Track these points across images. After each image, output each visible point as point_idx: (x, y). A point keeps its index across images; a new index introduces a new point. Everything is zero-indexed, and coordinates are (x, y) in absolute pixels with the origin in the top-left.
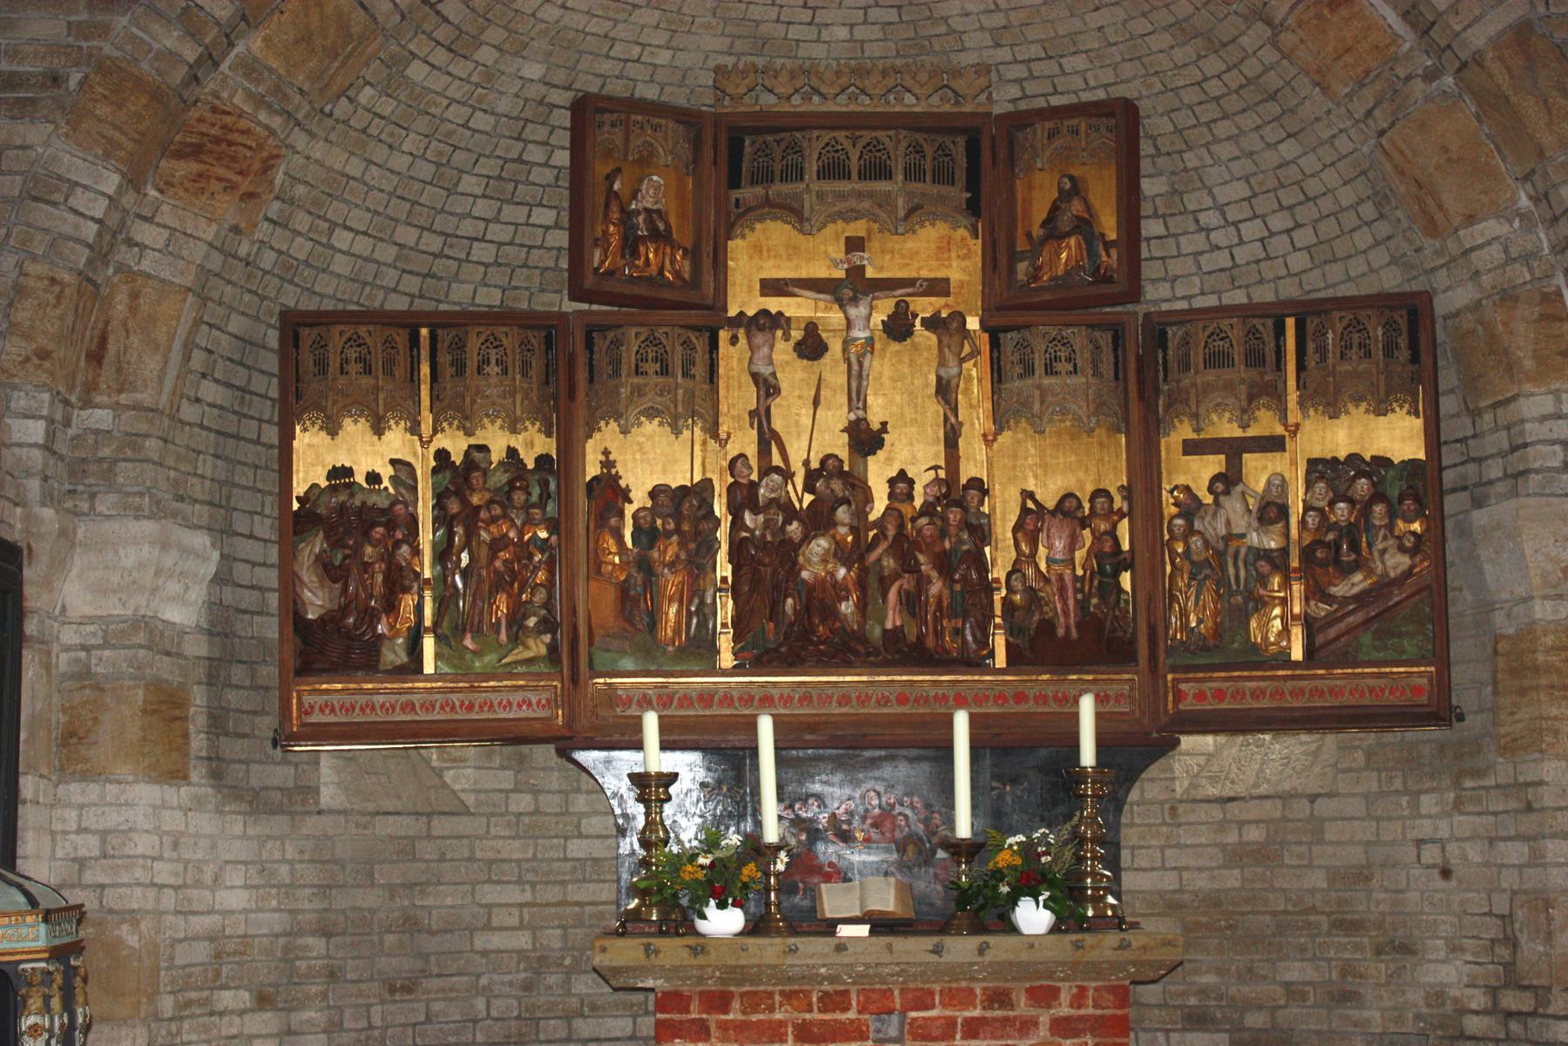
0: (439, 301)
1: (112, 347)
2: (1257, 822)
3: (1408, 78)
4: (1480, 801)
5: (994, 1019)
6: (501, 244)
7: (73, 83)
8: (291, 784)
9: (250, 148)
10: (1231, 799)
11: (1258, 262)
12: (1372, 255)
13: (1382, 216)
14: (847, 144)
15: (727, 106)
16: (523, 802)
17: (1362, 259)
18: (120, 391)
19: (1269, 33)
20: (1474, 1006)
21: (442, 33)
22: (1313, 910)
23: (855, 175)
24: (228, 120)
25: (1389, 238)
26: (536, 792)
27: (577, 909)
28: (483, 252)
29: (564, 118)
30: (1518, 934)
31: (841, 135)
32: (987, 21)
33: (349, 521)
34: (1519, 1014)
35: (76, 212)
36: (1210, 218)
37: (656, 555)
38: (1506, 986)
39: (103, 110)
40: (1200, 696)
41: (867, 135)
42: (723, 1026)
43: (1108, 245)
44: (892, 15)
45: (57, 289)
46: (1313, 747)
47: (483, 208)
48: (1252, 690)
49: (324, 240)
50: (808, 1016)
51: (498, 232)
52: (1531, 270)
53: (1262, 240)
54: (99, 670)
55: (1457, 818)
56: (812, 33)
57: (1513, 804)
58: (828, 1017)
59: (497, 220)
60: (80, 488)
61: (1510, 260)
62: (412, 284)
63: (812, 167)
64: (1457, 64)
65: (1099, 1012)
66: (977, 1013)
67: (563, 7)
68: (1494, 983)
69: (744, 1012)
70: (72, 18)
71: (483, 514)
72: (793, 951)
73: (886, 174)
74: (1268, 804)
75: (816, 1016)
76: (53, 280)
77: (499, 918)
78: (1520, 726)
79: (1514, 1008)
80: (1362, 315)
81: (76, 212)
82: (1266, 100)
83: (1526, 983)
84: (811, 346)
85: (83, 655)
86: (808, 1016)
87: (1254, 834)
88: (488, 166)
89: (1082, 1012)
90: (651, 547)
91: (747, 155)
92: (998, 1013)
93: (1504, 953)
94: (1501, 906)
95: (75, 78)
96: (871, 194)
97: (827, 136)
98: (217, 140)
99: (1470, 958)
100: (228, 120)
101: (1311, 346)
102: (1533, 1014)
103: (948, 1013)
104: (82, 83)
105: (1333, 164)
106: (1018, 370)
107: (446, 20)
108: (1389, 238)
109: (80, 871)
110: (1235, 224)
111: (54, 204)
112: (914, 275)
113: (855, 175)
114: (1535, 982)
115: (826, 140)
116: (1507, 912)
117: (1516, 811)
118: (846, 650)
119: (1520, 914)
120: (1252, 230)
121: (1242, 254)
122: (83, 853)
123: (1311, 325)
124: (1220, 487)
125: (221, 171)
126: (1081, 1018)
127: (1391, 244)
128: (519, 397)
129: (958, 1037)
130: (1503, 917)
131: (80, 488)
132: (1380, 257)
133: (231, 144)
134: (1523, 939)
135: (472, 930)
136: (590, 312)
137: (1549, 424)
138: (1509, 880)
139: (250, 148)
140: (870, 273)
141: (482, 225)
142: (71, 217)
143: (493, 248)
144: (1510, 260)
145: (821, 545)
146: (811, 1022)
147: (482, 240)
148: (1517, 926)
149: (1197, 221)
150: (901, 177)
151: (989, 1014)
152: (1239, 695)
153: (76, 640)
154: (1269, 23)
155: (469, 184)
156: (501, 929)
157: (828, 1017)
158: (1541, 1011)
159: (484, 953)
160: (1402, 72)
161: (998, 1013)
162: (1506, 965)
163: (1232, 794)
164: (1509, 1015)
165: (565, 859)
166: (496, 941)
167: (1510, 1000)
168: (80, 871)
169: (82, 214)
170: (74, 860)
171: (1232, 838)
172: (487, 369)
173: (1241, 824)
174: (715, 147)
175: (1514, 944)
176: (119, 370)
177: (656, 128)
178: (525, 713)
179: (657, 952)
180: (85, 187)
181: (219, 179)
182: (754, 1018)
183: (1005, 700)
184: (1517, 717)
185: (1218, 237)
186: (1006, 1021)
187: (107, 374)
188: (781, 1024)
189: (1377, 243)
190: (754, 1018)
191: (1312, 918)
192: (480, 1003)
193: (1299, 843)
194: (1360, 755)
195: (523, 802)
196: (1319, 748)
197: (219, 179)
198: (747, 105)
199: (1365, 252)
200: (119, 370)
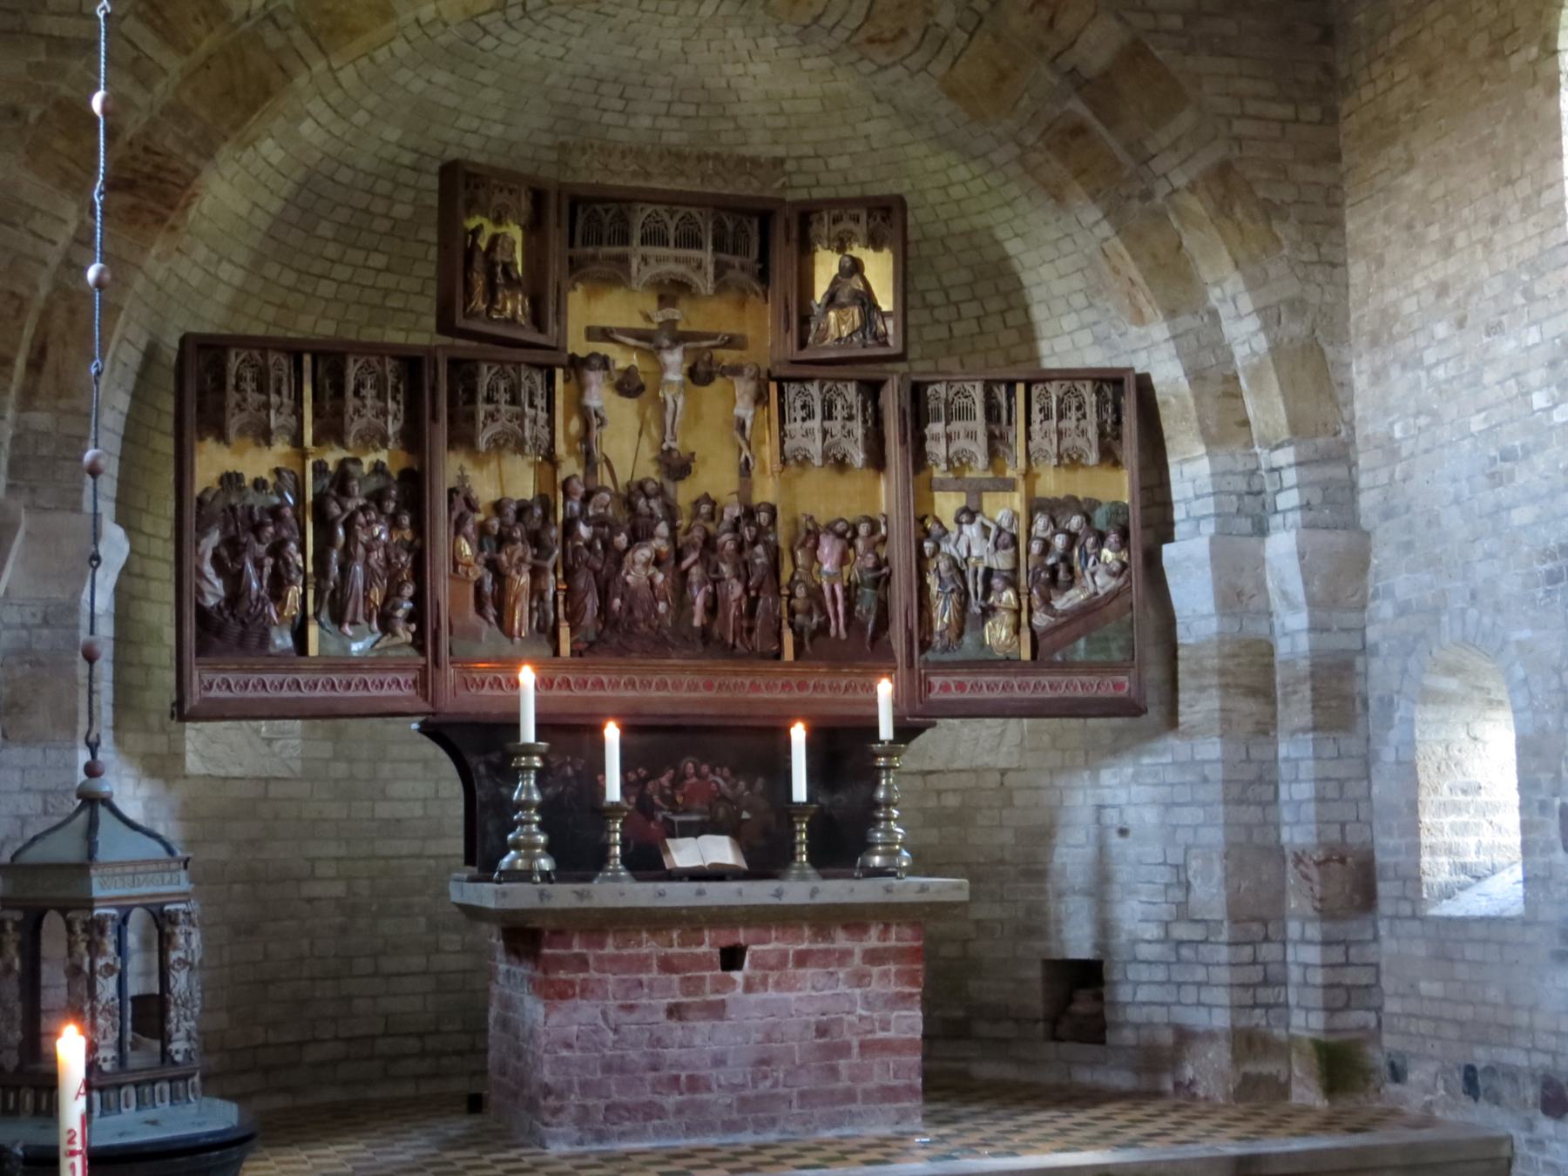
0: (288, 329)
1: (51, 356)
2: (955, 791)
3: (1128, 198)
4: (1157, 774)
5: (819, 951)
6: (341, 283)
7: (32, 118)
8: (165, 749)
9: (179, 186)
10: (931, 772)
11: (972, 336)
12: (1077, 336)
13: (1091, 305)
14: (666, 217)
15: (568, 178)
16: (340, 769)
17: (1067, 339)
18: (59, 397)
19: (1017, 151)
20: (1147, 936)
21: (335, 96)
22: (1002, 862)
23: (672, 243)
24: (158, 159)
25: (1095, 323)
26: (351, 761)
27: (382, 862)
28: (326, 288)
29: (432, 182)
30: (1192, 880)
31: (661, 209)
32: (769, 121)
33: (239, 521)
34: (1191, 942)
35: (34, 234)
36: (935, 298)
37: (504, 557)
38: (1178, 919)
39: (60, 144)
40: (945, 688)
41: (682, 211)
42: (599, 959)
43: (884, 315)
44: (691, 110)
45: (16, 303)
46: (999, 730)
47: (332, 250)
48: (989, 687)
49: (212, 270)
50: (670, 951)
51: (342, 272)
52: (1216, 357)
53: (978, 318)
54: (38, 647)
55: (1134, 789)
56: (620, 120)
57: (1189, 778)
58: (685, 951)
59: (340, 261)
60: (20, 483)
61: (1201, 347)
62: (270, 313)
63: (637, 234)
64: (1169, 189)
65: (900, 944)
66: (804, 946)
67: (429, 81)
68: (1166, 917)
69: (617, 947)
70: (31, 59)
71: (361, 518)
72: (700, 893)
73: (697, 244)
74: (964, 776)
75: (676, 950)
76: (13, 295)
77: (323, 869)
78: (1198, 716)
79: (1185, 937)
80: (1078, 385)
81: (34, 234)
82: (1001, 206)
83: (1198, 917)
84: (628, 386)
85: (24, 633)
86: (670, 951)
87: (951, 801)
88: (343, 215)
89: (887, 944)
90: (499, 550)
91: (585, 221)
92: (822, 946)
93: (1178, 895)
94: (1176, 856)
95: (34, 114)
96: (687, 261)
97: (649, 209)
98: (149, 177)
99: (1144, 899)
100: (158, 159)
101: (1035, 407)
102: (1205, 941)
103: (781, 946)
104: (42, 117)
105: (1052, 261)
106: (801, 414)
107: (340, 86)
108: (1095, 323)
109: (22, 827)
110: (956, 304)
111: (13, 224)
112: (715, 330)
113: (672, 243)
114: (1207, 917)
115: (648, 211)
116: (1181, 861)
117: (1192, 784)
118: (660, 644)
119: (1195, 864)
120: (969, 310)
121: (959, 328)
122: (25, 810)
123: (1035, 392)
124: (964, 518)
125: (152, 204)
126: (886, 950)
127: (1097, 329)
128: (390, 418)
129: (790, 965)
130: (1177, 866)
131: (20, 483)
132: (1085, 337)
133: (161, 181)
134: (1196, 883)
135: (299, 880)
136: (452, 347)
137: (1229, 478)
138: (1183, 836)
139: (179, 186)
140: (681, 327)
141: (328, 265)
142: (30, 239)
143: (334, 286)
144: (1201, 347)
145: (644, 553)
146: (673, 955)
147: (328, 278)
148: (1190, 873)
149: (924, 299)
150: (710, 248)
151: (815, 947)
152: (961, 686)
153: (17, 619)
154: (1020, 145)
155: (325, 229)
156: (322, 879)
157: (685, 951)
158: (1212, 939)
159: (310, 900)
160: (1123, 192)
161: (822, 946)
162: (1178, 904)
163: (931, 768)
164: (1180, 943)
165: (373, 819)
166: (317, 889)
167: (1181, 931)
168: (22, 827)
169: (40, 237)
170: (17, 817)
171: (931, 803)
172: (363, 392)
173: (939, 793)
174: (559, 212)
175: (1188, 887)
176: (58, 376)
177: (511, 191)
178: (394, 692)
179: (549, 897)
180: (43, 213)
181: (152, 212)
182: (625, 952)
183: (735, 684)
184: (1196, 708)
185: (940, 314)
186: (827, 952)
187: (46, 382)
188: (647, 957)
189: (1082, 328)
190: (625, 952)
191: (1001, 868)
192: (305, 943)
193: (990, 807)
194: (1046, 738)
195: (340, 769)
196: (1003, 732)
197: (152, 212)
198: (583, 177)
199: (1070, 333)
200: (58, 376)
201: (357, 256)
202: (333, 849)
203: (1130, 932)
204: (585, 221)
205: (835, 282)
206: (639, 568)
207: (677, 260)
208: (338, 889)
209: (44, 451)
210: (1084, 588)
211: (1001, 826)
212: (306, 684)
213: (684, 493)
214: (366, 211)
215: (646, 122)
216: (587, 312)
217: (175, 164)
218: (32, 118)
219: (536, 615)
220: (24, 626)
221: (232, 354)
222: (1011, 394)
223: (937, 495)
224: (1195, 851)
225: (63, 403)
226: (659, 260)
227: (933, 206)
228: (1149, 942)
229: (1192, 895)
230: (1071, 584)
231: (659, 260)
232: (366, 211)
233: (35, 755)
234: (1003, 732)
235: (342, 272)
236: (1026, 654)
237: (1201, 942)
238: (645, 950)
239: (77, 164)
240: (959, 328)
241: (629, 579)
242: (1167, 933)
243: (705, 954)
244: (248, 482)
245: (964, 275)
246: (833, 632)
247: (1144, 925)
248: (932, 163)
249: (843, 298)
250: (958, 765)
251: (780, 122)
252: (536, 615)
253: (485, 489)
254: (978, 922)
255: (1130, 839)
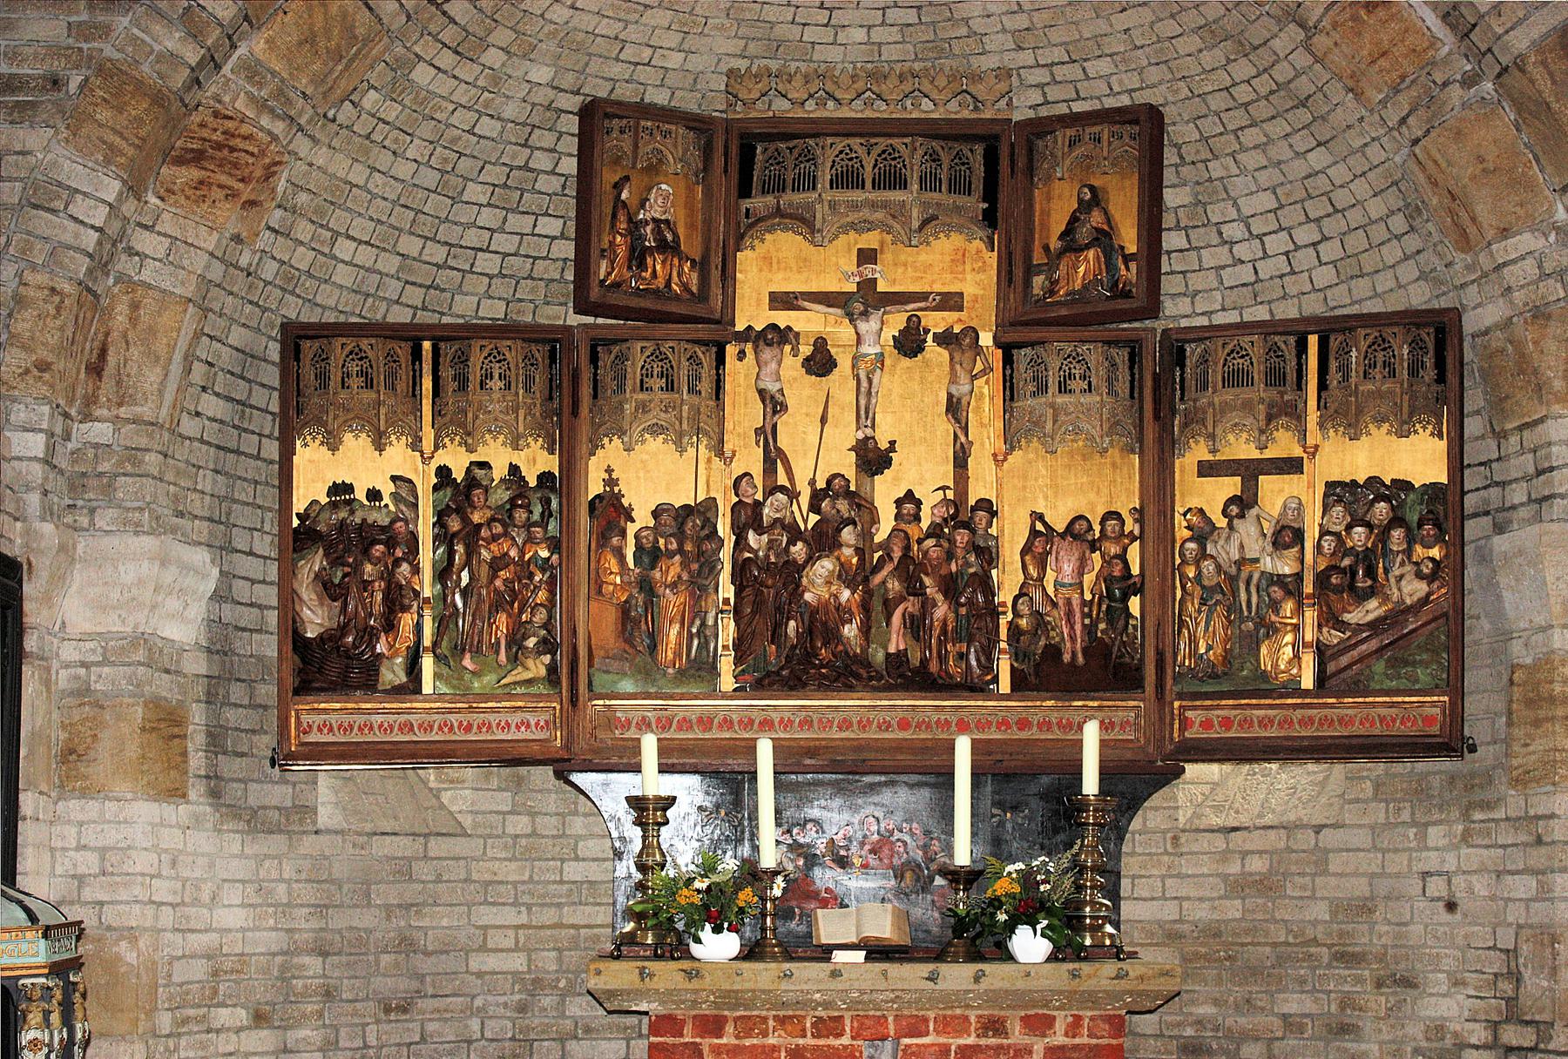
0: (442, 314)
1: (112, 359)
2: (1261, 852)
3: (1445, 84)
7: (73, 87)
9: (252, 154)
11: (1281, 277)
12: (1400, 270)
14: (861, 151)
17: (1390, 274)
20: (1474, 1041)
23: (868, 184)
25: (1418, 252)
26: (533, 814)
29: (572, 124)
31: (855, 142)
32: (1009, 23)
33: (344, 540)
36: (1234, 231)
38: (1508, 1020)
39: (103, 115)
40: (1207, 724)
41: (883, 143)
43: (1127, 259)
45: (57, 299)
46: (1320, 777)
47: (488, 217)
49: (327, 251)
50: (801, 1041)
51: (503, 243)
56: (827, 35)
58: (822, 1042)
63: (825, 176)
64: (1497, 69)
70: (73, 19)
71: (484, 533)
72: (788, 976)
73: (900, 183)
74: (1272, 834)
75: (809, 1041)
79: (1514, 1043)
81: (76, 220)
83: (1528, 1018)
85: (82, 671)
86: (801, 1041)
87: (1257, 865)
88: (494, 174)
89: (1077, 1041)
91: (754, 162)
92: (993, 1041)
93: (1506, 987)
94: (1506, 939)
96: (885, 205)
97: (841, 143)
98: (219, 146)
99: (1472, 993)
100: (230, 124)
101: (1333, 365)
103: (942, 1040)
106: (1031, 388)
110: (1260, 237)
111: (53, 211)
113: (868, 184)
114: (1537, 1018)
117: (1526, 845)
118: (849, 674)
123: (1334, 343)
124: (1234, 510)
125: (223, 179)
131: (80, 503)
133: (232, 150)
139: (252, 154)
141: (487, 234)
142: (71, 225)
144: (1544, 276)
148: (1521, 960)
151: (983, 1042)
152: (1246, 723)
155: (475, 192)
157: (822, 1042)
159: (480, 975)
161: (993, 1041)
162: (1508, 1000)
166: (492, 962)
170: (74, 876)
171: (1234, 868)
172: (490, 384)
173: (1245, 854)
174: (726, 155)
175: (1518, 979)
176: (119, 383)
178: (523, 734)
179: (651, 975)
182: (747, 1042)
185: (1241, 251)
187: (107, 387)
192: (475, 1024)
195: (520, 824)
196: (1327, 778)
200: (119, 383)
201: (515, 222)
202: (510, 916)
203: (1456, 1034)
204: (754, 162)
205: (1074, 220)
206: (820, 581)
207: (874, 205)
208: (518, 962)
209: (105, 467)
210: (1386, 599)
211: (1313, 897)
212: (420, 726)
213: (885, 492)
214: (526, 167)
215: (859, 35)
216: (767, 271)
217: (245, 129)
218: (73, 87)
219: (696, 642)
220: (84, 664)
221: (1332, 339)
222: (1302, 347)
223: (1261, 477)
224: (1526, 933)
225: (123, 412)
226: (855, 207)
227: (1217, 114)
228: (1477, 1047)
229: (1522, 990)
230: (1371, 593)
231: (855, 207)
232: (526, 167)
233: (93, 808)
234: (1327, 778)
235: (503, 243)
236: (1308, 682)
237: (1531, 1049)
238: (771, 1040)
239: (121, 135)
240: (1266, 269)
241: (808, 596)
242: (1496, 1038)
243: (845, 1047)
244: (360, 495)
245: (1267, 201)
246: (1067, 658)
247: (1471, 1025)
248: (1208, 59)
249: (1083, 234)
250: (1269, 819)
251: (1021, 21)
252: (696, 642)
253: (642, 501)
254: (1285, 1017)
255: (1458, 916)
